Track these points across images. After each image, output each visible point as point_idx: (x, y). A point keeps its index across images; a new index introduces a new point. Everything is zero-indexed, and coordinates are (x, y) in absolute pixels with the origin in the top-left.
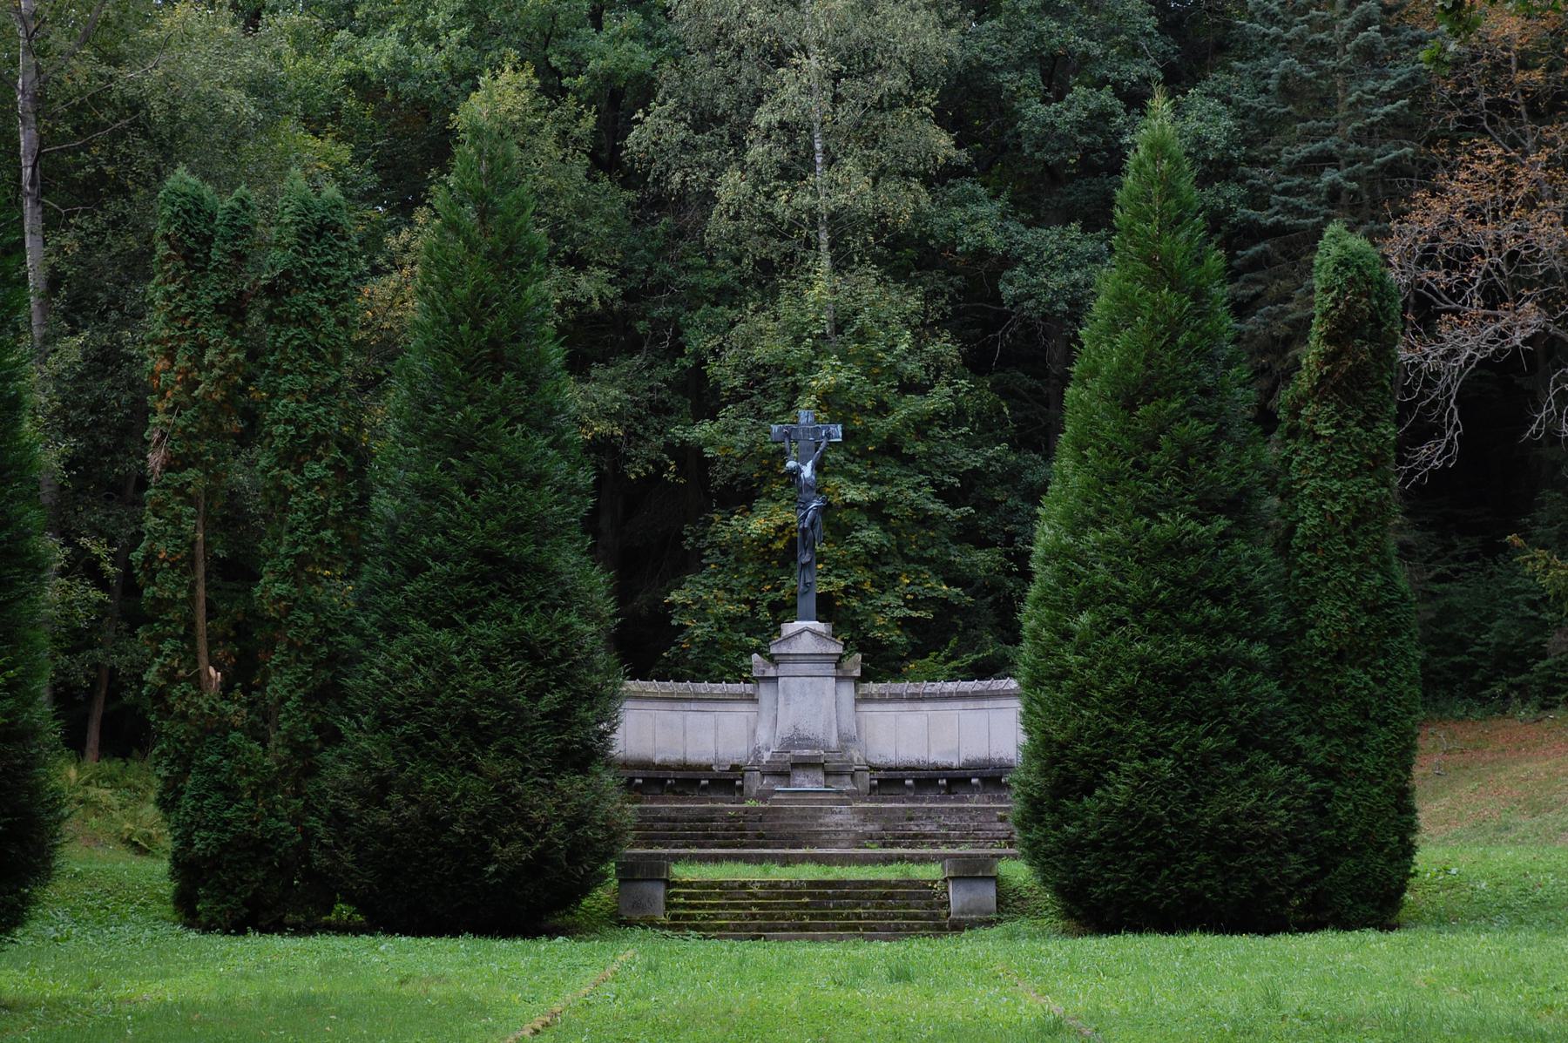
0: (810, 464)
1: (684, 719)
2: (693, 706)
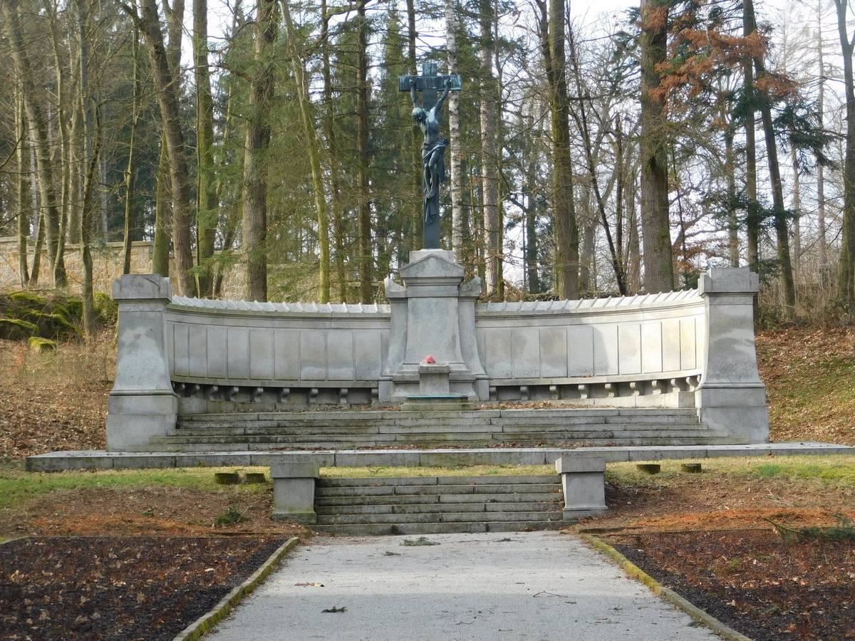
0: (433, 110)
1: (325, 336)
2: (333, 324)
